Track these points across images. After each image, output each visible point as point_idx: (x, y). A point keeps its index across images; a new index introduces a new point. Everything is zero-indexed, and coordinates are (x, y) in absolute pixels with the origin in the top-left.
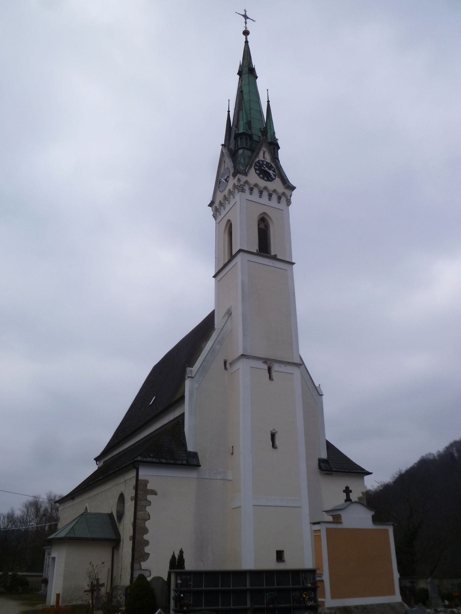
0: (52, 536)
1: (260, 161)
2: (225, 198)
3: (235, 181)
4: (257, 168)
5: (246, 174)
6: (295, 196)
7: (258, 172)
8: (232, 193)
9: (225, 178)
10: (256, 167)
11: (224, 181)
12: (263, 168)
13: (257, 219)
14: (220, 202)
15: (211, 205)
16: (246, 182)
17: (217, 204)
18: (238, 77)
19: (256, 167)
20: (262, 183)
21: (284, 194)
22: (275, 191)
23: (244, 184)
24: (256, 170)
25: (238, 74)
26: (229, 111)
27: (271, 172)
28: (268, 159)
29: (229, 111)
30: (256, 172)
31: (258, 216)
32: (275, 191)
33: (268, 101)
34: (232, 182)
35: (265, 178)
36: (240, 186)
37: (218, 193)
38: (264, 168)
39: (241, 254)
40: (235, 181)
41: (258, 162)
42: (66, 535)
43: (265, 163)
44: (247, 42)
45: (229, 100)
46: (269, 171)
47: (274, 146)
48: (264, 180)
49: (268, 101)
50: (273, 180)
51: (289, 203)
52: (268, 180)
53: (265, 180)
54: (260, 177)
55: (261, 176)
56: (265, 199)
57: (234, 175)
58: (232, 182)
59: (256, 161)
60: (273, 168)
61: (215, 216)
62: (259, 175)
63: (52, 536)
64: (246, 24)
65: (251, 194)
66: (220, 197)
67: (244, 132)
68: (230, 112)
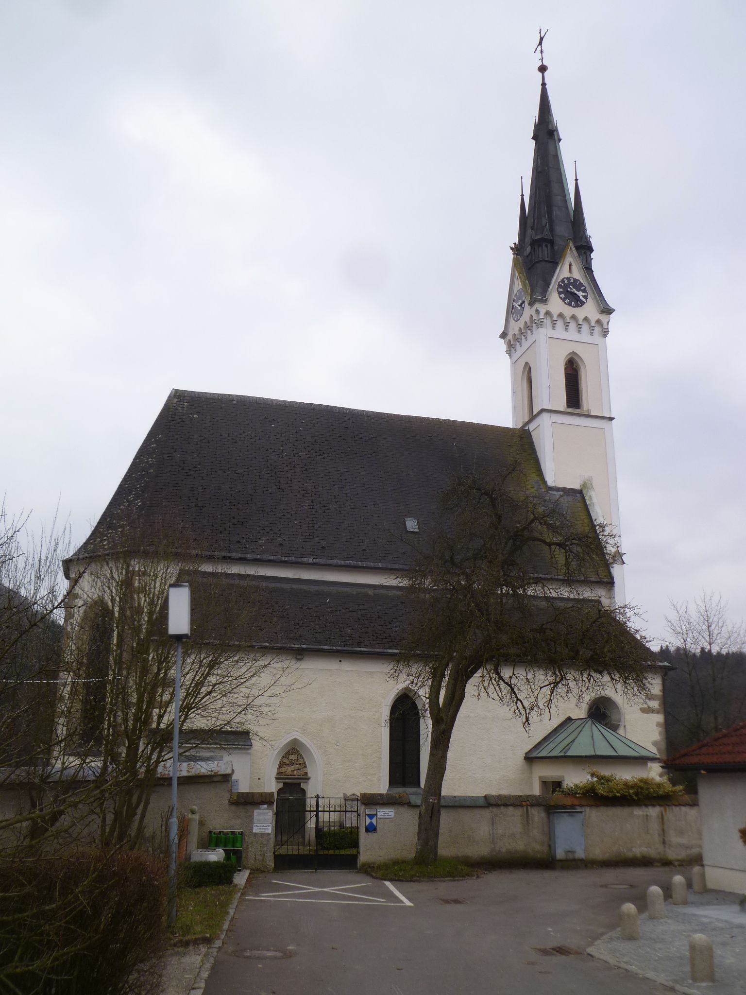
0: (158, 749)
1: (565, 280)
2: (522, 333)
3: (532, 311)
4: (561, 290)
5: (545, 301)
6: (614, 322)
7: (562, 296)
8: (530, 328)
9: (520, 303)
10: (559, 289)
11: (519, 308)
12: (569, 289)
13: (564, 360)
14: (515, 335)
15: (504, 335)
16: (548, 313)
17: (510, 336)
18: (534, 142)
19: (559, 289)
20: (568, 311)
21: (599, 322)
22: (586, 319)
23: (364, 865)
24: (560, 293)
25: (533, 138)
26: (522, 195)
27: (580, 294)
28: (577, 274)
29: (522, 195)
30: (560, 297)
31: (568, 354)
32: (586, 319)
33: (576, 180)
34: (528, 312)
35: (573, 303)
36: (539, 320)
37: (512, 322)
38: (572, 289)
39: (545, 415)
40: (532, 311)
41: (562, 281)
42: (678, 991)
43: (572, 281)
44: (544, 84)
45: (522, 177)
46: (577, 293)
47: (585, 249)
48: (572, 306)
49: (576, 180)
50: (583, 303)
51: (605, 333)
52: (577, 306)
53: (573, 307)
54: (566, 304)
55: (567, 301)
56: (572, 334)
57: (531, 304)
58: (528, 312)
59: (559, 280)
60: (584, 286)
61: (509, 352)
62: (564, 300)
63: (158, 749)
64: (542, 53)
65: (554, 328)
66: (515, 327)
67: (542, 238)
68: (524, 195)
